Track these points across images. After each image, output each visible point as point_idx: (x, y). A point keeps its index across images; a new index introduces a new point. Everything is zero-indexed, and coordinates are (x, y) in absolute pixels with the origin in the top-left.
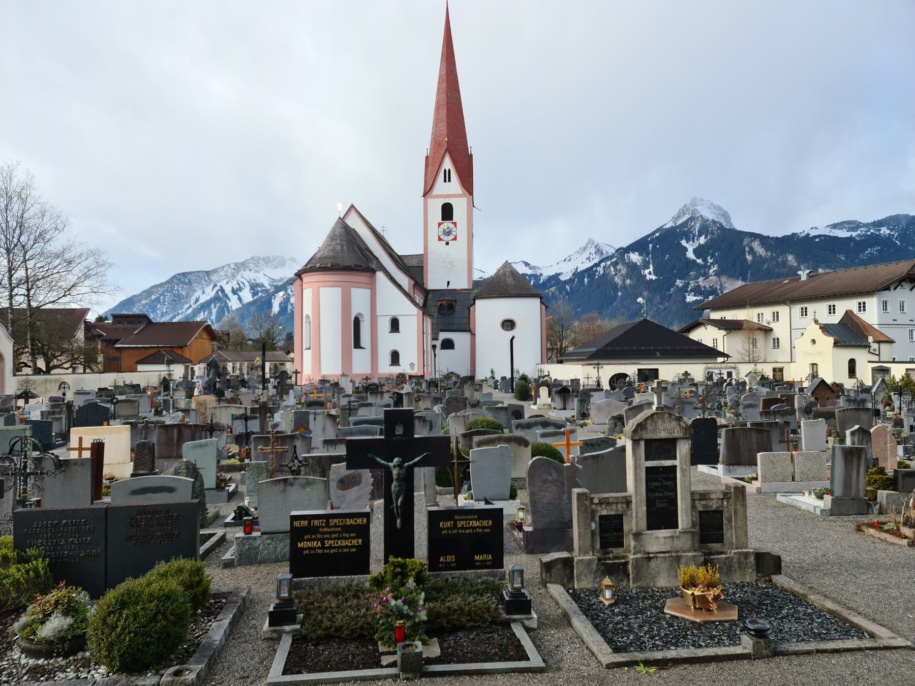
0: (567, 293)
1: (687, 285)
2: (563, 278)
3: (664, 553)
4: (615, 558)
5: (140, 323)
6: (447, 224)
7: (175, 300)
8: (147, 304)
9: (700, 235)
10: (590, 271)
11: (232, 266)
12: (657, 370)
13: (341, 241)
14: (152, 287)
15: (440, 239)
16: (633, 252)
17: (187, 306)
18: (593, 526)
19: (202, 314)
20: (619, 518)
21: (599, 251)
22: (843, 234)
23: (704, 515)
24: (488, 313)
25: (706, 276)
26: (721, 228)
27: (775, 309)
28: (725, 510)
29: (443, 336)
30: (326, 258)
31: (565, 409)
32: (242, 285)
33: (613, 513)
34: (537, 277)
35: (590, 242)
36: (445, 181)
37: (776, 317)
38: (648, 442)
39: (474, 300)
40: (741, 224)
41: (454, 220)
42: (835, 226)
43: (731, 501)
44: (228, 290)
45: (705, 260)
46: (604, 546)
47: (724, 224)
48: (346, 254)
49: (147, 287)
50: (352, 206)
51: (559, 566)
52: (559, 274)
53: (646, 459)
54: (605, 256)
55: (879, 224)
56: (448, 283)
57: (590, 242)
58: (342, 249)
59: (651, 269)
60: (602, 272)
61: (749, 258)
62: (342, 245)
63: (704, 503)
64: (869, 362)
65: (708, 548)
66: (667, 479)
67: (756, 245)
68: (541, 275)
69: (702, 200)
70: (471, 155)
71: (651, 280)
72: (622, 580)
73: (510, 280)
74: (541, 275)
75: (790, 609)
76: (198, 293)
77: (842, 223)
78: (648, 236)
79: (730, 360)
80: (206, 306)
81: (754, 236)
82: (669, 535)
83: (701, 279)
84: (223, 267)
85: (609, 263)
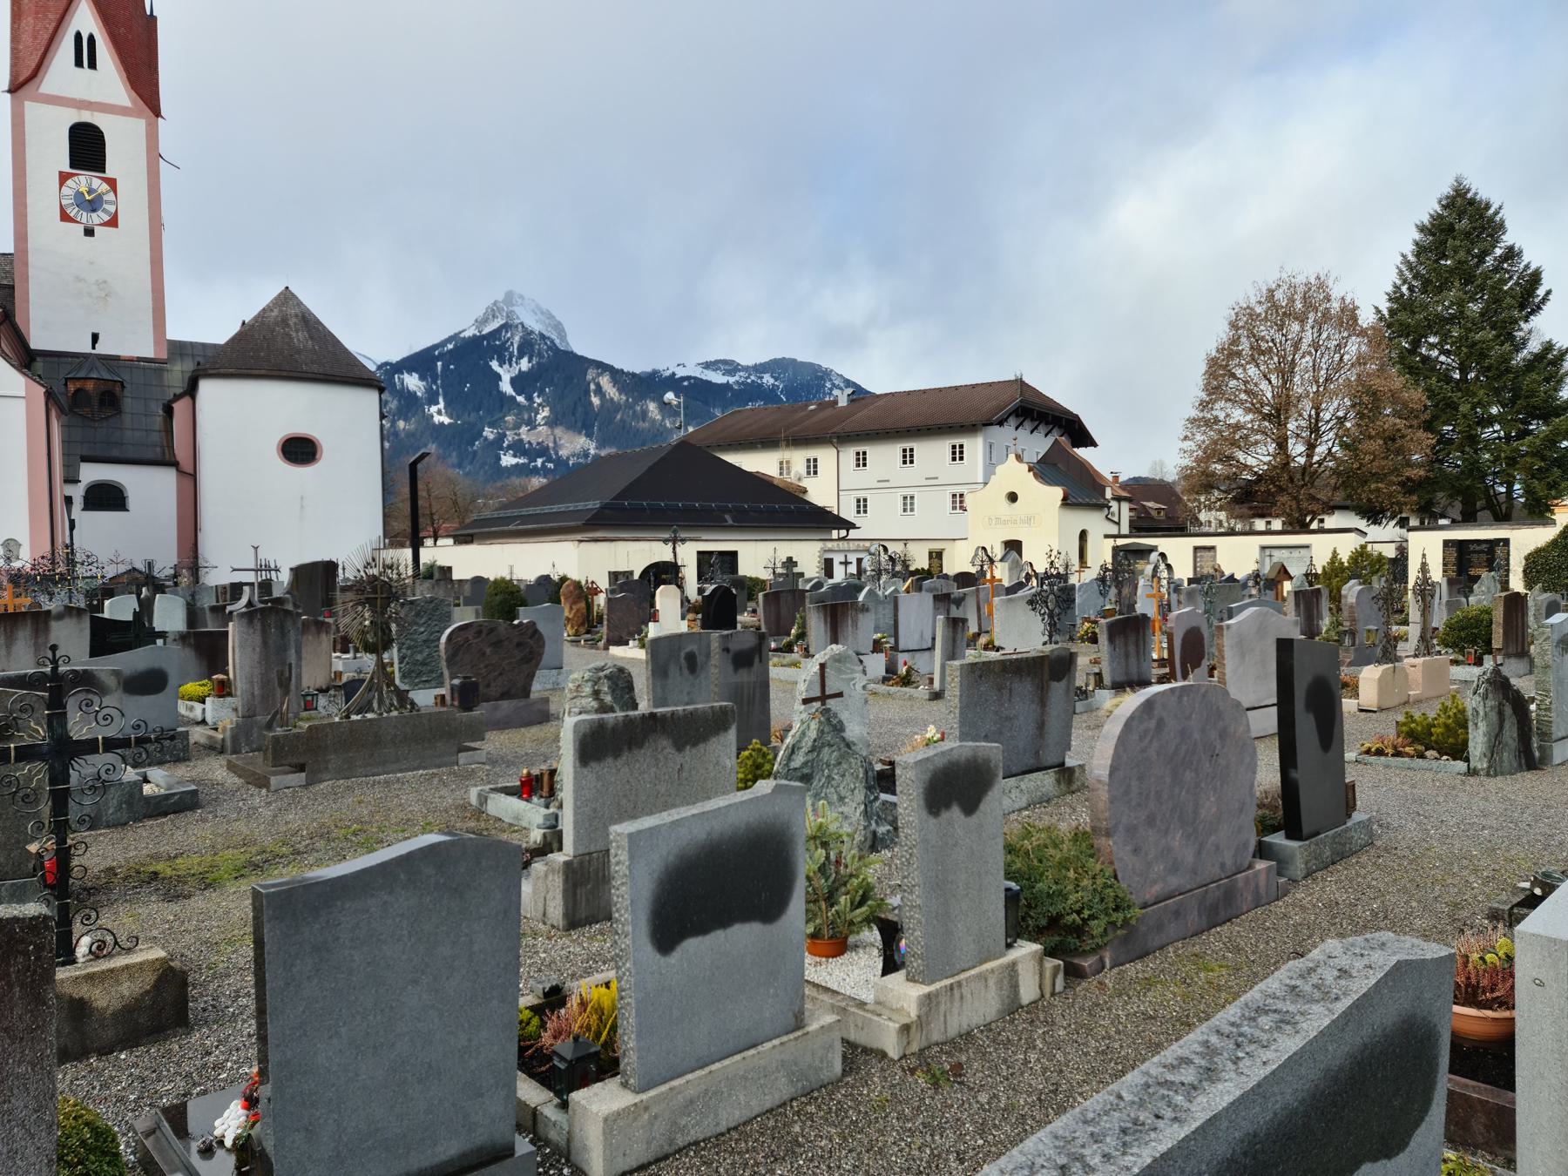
1: (502, 437)
6: (85, 181)
9: (520, 357)
12: (734, 554)
15: (65, 217)
16: (410, 372)
22: (718, 378)
25: (532, 425)
26: (553, 347)
27: (812, 453)
29: (92, 473)
36: (79, 63)
37: (812, 467)
40: (581, 345)
41: (109, 173)
42: (707, 365)
45: (530, 399)
47: (557, 342)
55: (760, 369)
59: (441, 405)
61: (596, 401)
64: (1107, 536)
67: (605, 381)
69: (521, 297)
70: (152, 20)
71: (442, 424)
73: (300, 337)
77: (717, 362)
78: (435, 347)
79: (853, 534)
81: (603, 367)
83: (524, 429)
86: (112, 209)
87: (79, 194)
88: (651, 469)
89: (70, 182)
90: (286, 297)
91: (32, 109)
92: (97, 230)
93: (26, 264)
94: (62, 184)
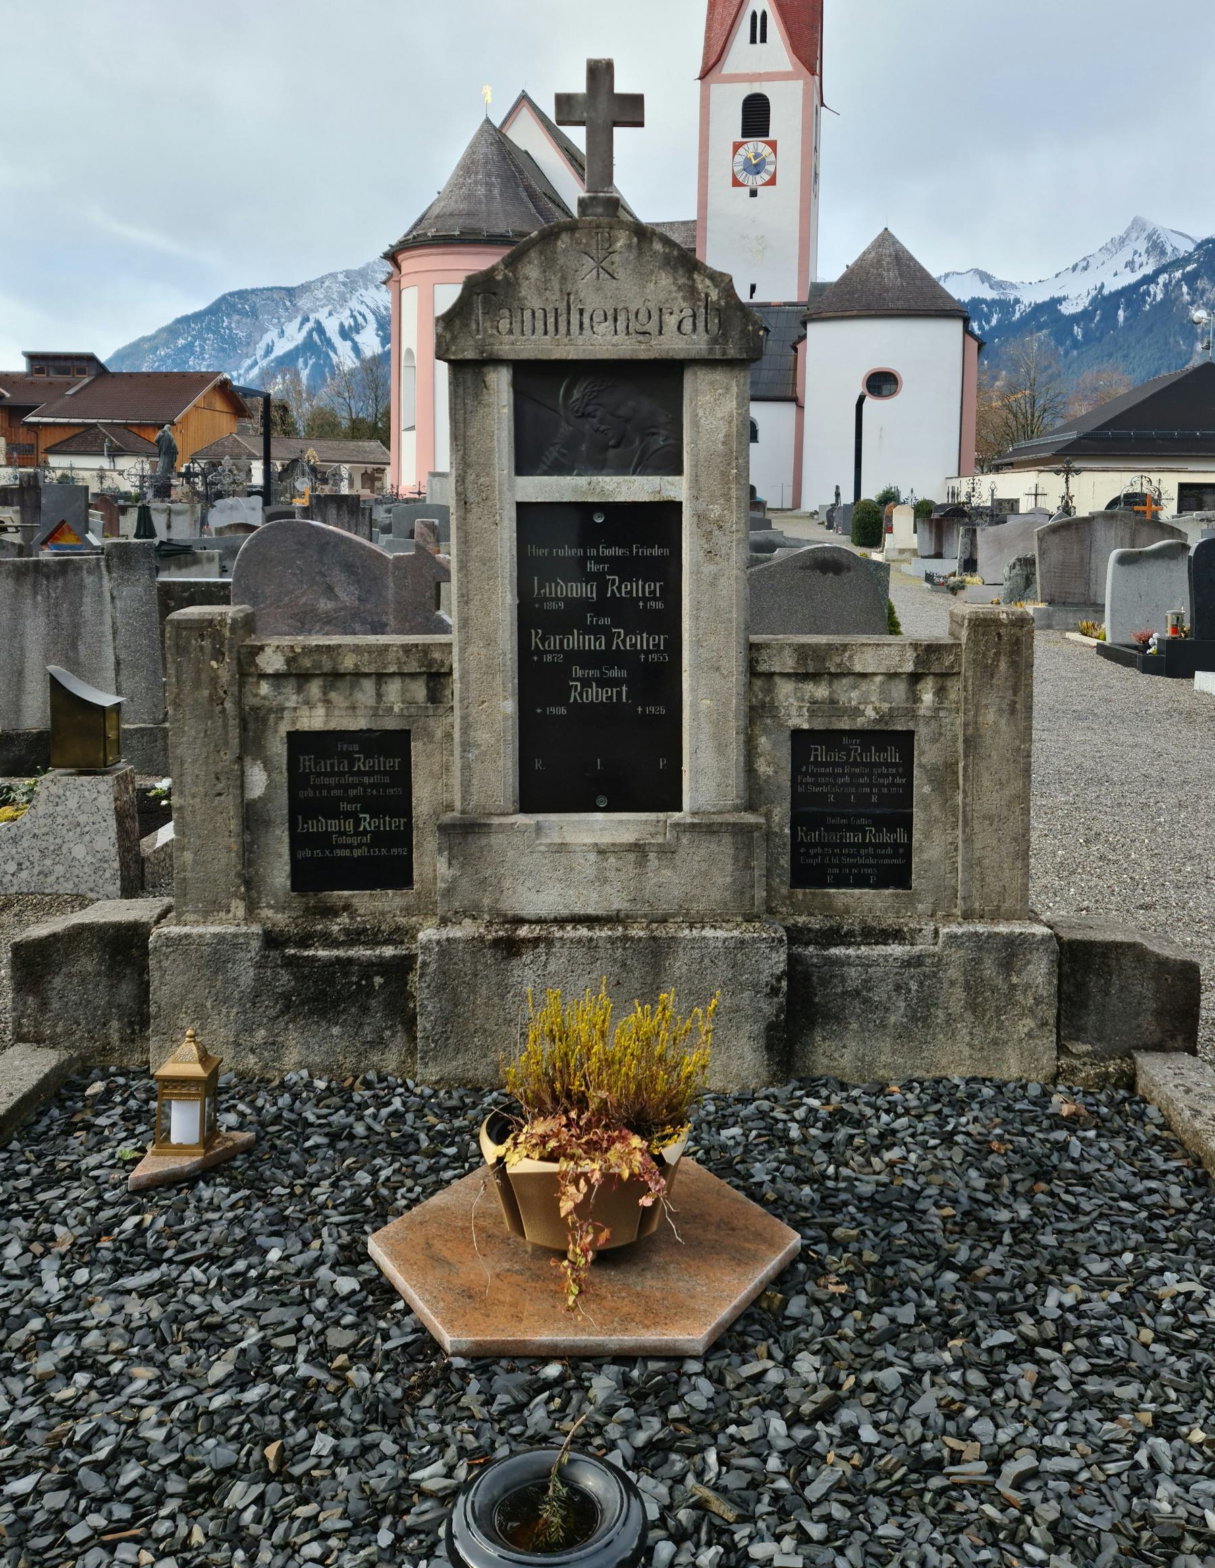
0: (1076, 344)
2: (1067, 309)
3: (590, 921)
4: (355, 937)
5: (82, 371)
6: (755, 146)
7: (224, 350)
8: (168, 356)
10: (1132, 295)
11: (341, 278)
12: (679, 471)
13: (488, 175)
14: (179, 321)
15: (736, 183)
17: (249, 362)
18: (258, 780)
19: (279, 379)
20: (393, 746)
21: (1156, 246)
23: (820, 753)
24: (835, 356)
28: (923, 733)
30: (452, 215)
31: (939, 555)
32: (360, 319)
33: (360, 723)
34: (1006, 306)
35: (1137, 224)
36: (753, 41)
38: (532, 375)
39: (804, 324)
41: (772, 137)
43: (955, 690)
44: (331, 328)
46: (312, 874)
48: (497, 205)
49: (168, 320)
50: (524, 98)
51: (88, 964)
52: (1059, 301)
53: (525, 464)
54: (1169, 258)
56: (753, 288)
57: (1137, 224)
58: (489, 197)
60: (1159, 297)
62: (489, 186)
63: (821, 691)
65: (828, 909)
66: (627, 568)
68: (1017, 301)
72: (380, 1043)
73: (891, 276)
74: (1017, 301)
75: (1102, 1284)
76: (271, 335)
80: (287, 362)
82: (628, 837)
84: (322, 280)
85: (1178, 274)
86: (771, 168)
87: (748, 160)
88: (1152, 396)
89: (741, 151)
90: (886, 238)
91: (716, 89)
92: (760, 190)
93: (705, 229)
94: (735, 153)
